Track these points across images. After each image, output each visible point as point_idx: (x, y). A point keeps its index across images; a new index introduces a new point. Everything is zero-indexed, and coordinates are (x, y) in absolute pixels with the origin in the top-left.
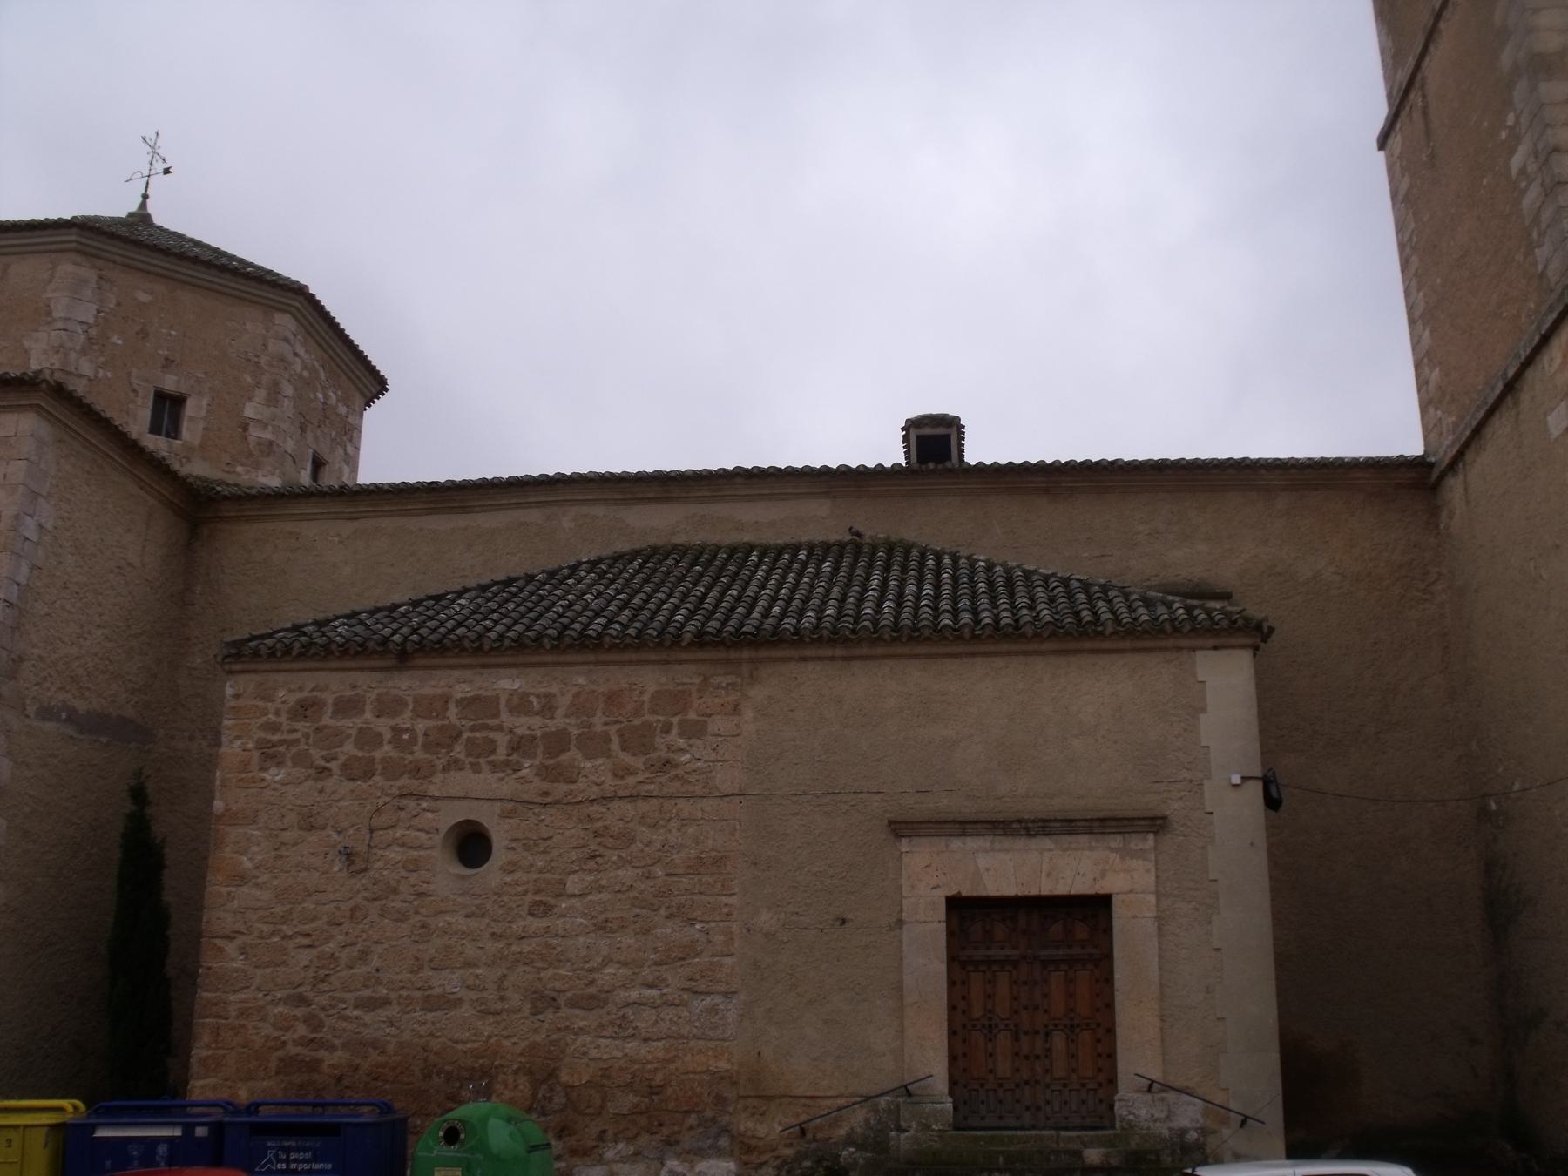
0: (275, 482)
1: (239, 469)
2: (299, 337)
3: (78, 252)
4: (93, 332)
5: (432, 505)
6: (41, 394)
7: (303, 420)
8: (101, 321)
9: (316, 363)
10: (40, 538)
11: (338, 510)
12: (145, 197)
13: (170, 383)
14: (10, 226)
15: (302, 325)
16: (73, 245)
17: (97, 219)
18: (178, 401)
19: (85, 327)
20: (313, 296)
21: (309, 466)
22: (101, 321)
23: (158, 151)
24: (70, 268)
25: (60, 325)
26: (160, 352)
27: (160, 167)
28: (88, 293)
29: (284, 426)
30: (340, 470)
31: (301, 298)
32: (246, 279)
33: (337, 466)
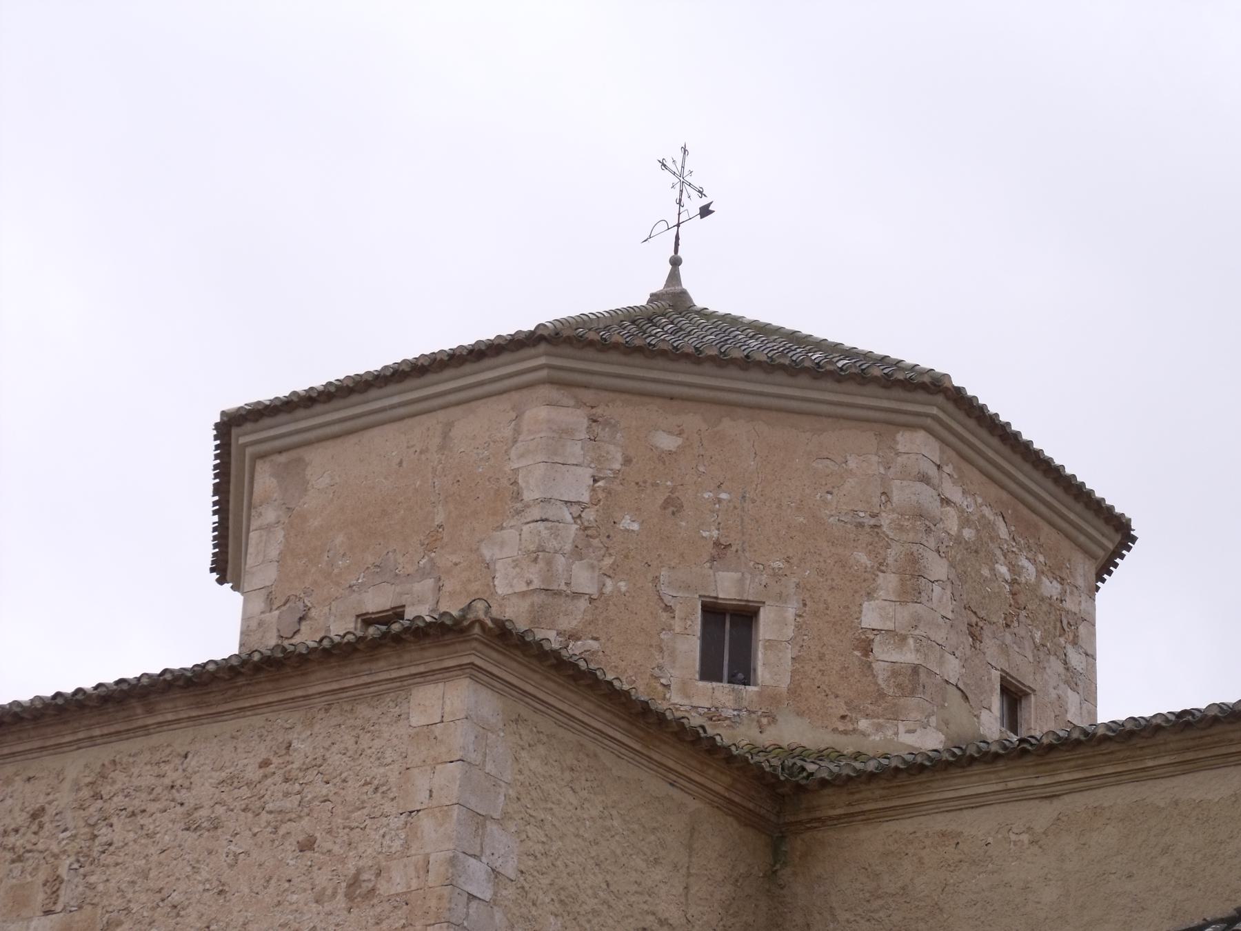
0: (930, 741)
1: (863, 724)
2: (948, 469)
3: (552, 382)
4: (590, 515)
5: (1190, 756)
6: (475, 644)
7: (974, 619)
8: (601, 495)
9: (987, 511)
10: (495, 894)
11: (1021, 783)
12: (676, 262)
13: (727, 587)
14: (465, 353)
15: (948, 445)
16: (543, 373)
17: (583, 321)
18: (745, 616)
19: (576, 510)
20: (959, 391)
21: (996, 702)
22: (601, 495)
23: (688, 179)
24: (543, 412)
25: (536, 513)
26: (705, 534)
27: (693, 204)
28: (575, 450)
29: (939, 636)
30: (1060, 700)
31: (940, 399)
32: (815, 378)
33: (1053, 694)
